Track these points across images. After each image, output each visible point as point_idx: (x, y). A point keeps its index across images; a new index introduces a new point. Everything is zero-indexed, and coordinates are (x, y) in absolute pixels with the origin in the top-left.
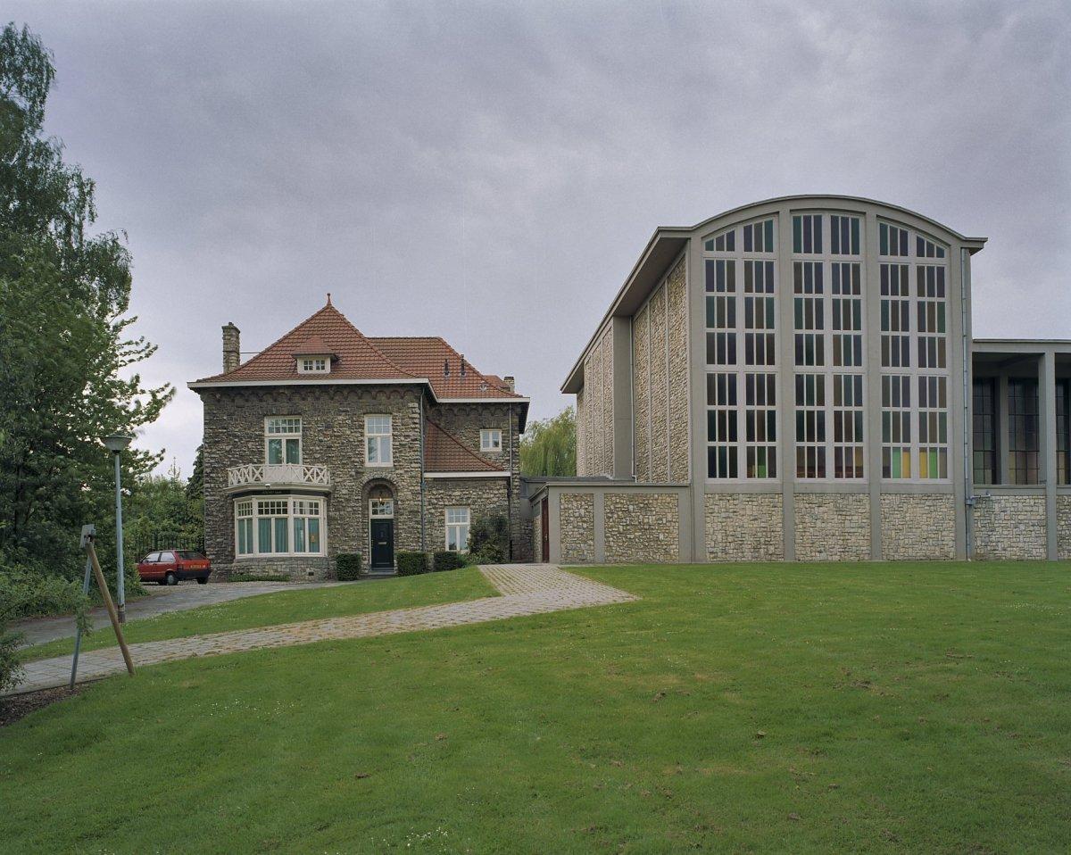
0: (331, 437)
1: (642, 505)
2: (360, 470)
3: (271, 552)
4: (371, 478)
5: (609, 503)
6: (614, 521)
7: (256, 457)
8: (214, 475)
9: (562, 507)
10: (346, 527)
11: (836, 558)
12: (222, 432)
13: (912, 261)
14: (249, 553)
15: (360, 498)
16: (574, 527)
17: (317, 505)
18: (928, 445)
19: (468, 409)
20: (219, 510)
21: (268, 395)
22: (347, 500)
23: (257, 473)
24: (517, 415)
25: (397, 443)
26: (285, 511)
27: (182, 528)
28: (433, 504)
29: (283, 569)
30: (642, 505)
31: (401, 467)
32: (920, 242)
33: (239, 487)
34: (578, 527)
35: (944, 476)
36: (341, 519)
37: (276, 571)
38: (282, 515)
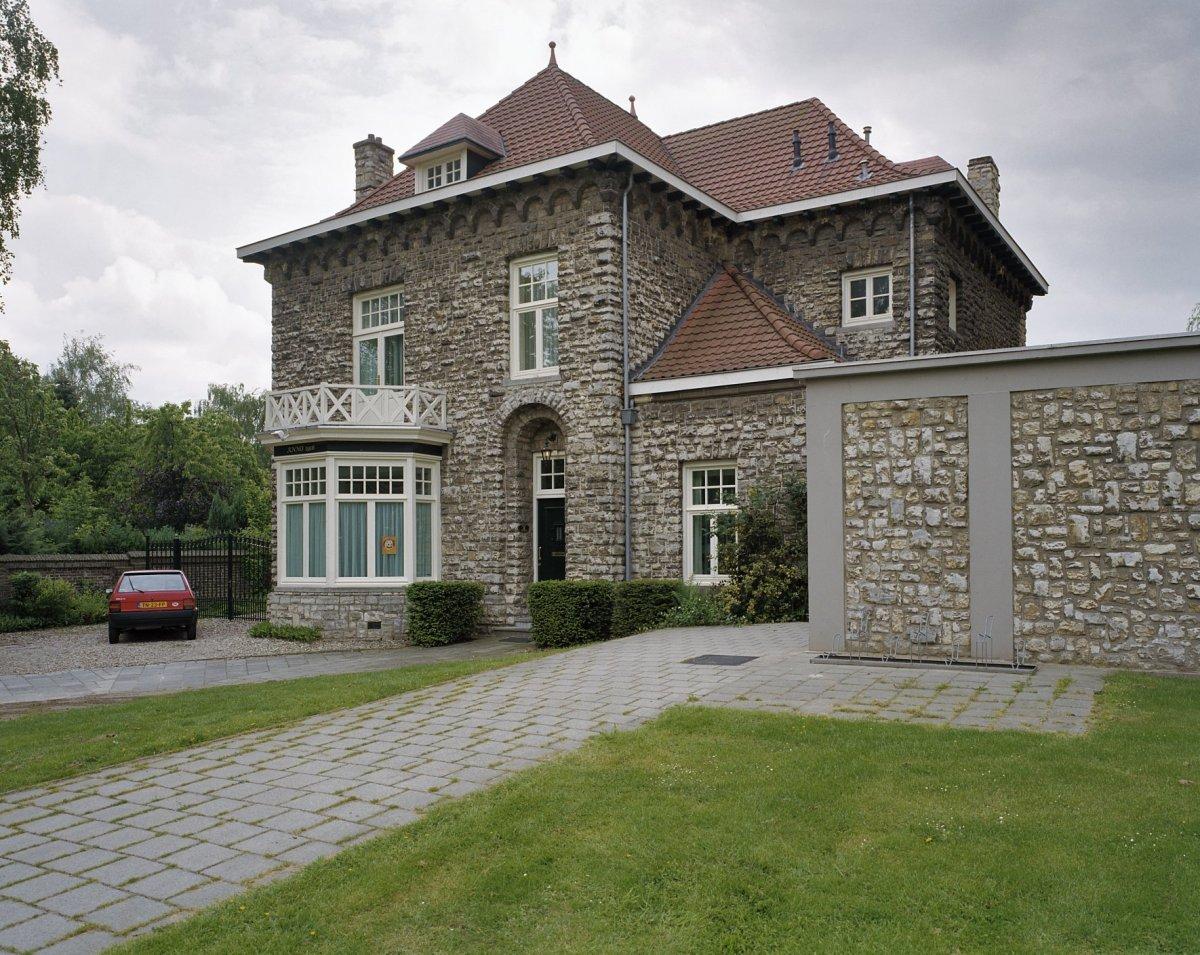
1: (1178, 430)
2: (497, 389)
4: (516, 405)
5: (1032, 427)
6: (1050, 499)
9: (851, 451)
14: (312, 574)
15: (497, 452)
16: (893, 524)
17: (428, 472)
19: (810, 228)
22: (475, 458)
23: (338, 404)
24: (930, 222)
26: (398, 488)
30: (1178, 430)
34: (910, 523)
36: (465, 501)
38: (391, 497)
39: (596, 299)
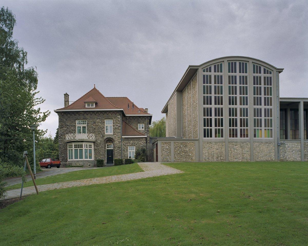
0: (95, 126)
1: (185, 145)
2: (104, 135)
3: (78, 159)
4: (107, 137)
5: (175, 145)
6: (176, 150)
7: (74, 132)
8: (62, 137)
9: (162, 146)
10: (100, 151)
11: (241, 161)
12: (64, 124)
13: (262, 75)
14: (71, 159)
15: (103, 143)
16: (165, 152)
17: (91, 145)
18: (267, 128)
19: (135, 118)
20: (63, 147)
21: (77, 114)
22: (100, 144)
23: (74, 136)
24: (149, 119)
25: (114, 128)
26: (82, 147)
27: (52, 152)
28: (125, 145)
29: (81, 164)
30: (185, 145)
31: (115, 134)
32: (265, 70)
33: (69, 140)
34: (166, 152)
35: (272, 137)
36: (98, 149)
37: (79, 164)
38: (81, 148)
39: (119, 126)
